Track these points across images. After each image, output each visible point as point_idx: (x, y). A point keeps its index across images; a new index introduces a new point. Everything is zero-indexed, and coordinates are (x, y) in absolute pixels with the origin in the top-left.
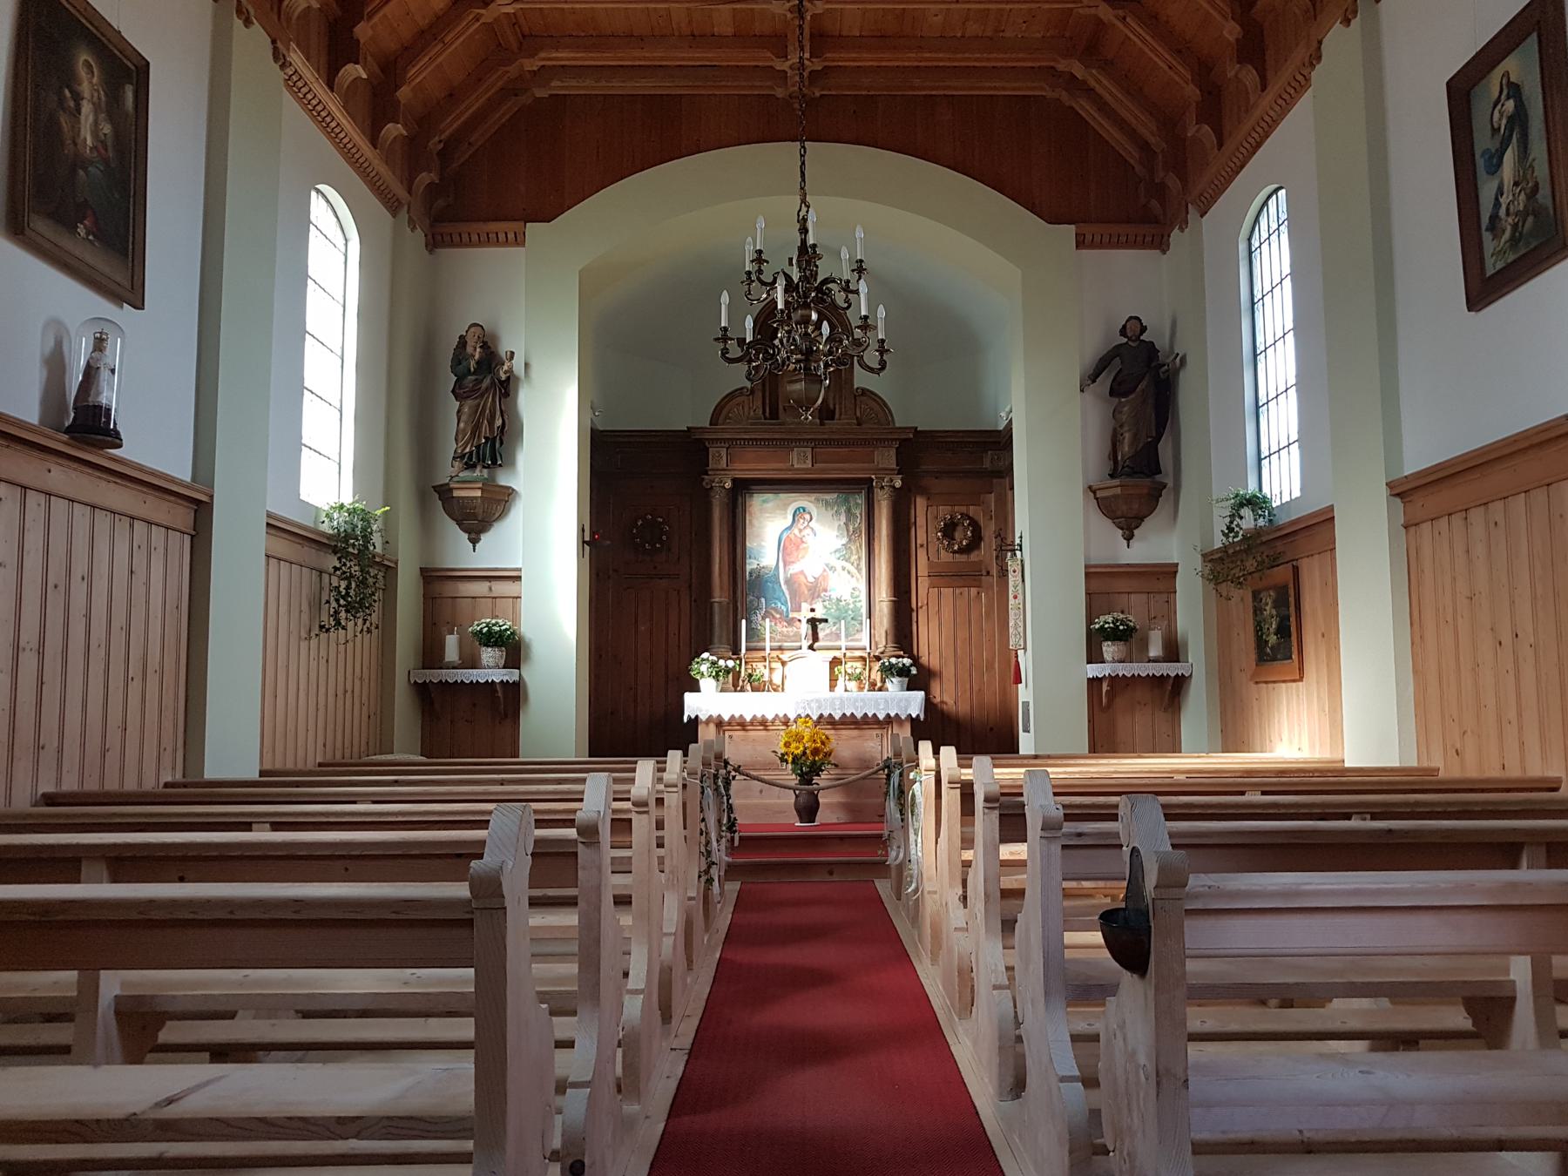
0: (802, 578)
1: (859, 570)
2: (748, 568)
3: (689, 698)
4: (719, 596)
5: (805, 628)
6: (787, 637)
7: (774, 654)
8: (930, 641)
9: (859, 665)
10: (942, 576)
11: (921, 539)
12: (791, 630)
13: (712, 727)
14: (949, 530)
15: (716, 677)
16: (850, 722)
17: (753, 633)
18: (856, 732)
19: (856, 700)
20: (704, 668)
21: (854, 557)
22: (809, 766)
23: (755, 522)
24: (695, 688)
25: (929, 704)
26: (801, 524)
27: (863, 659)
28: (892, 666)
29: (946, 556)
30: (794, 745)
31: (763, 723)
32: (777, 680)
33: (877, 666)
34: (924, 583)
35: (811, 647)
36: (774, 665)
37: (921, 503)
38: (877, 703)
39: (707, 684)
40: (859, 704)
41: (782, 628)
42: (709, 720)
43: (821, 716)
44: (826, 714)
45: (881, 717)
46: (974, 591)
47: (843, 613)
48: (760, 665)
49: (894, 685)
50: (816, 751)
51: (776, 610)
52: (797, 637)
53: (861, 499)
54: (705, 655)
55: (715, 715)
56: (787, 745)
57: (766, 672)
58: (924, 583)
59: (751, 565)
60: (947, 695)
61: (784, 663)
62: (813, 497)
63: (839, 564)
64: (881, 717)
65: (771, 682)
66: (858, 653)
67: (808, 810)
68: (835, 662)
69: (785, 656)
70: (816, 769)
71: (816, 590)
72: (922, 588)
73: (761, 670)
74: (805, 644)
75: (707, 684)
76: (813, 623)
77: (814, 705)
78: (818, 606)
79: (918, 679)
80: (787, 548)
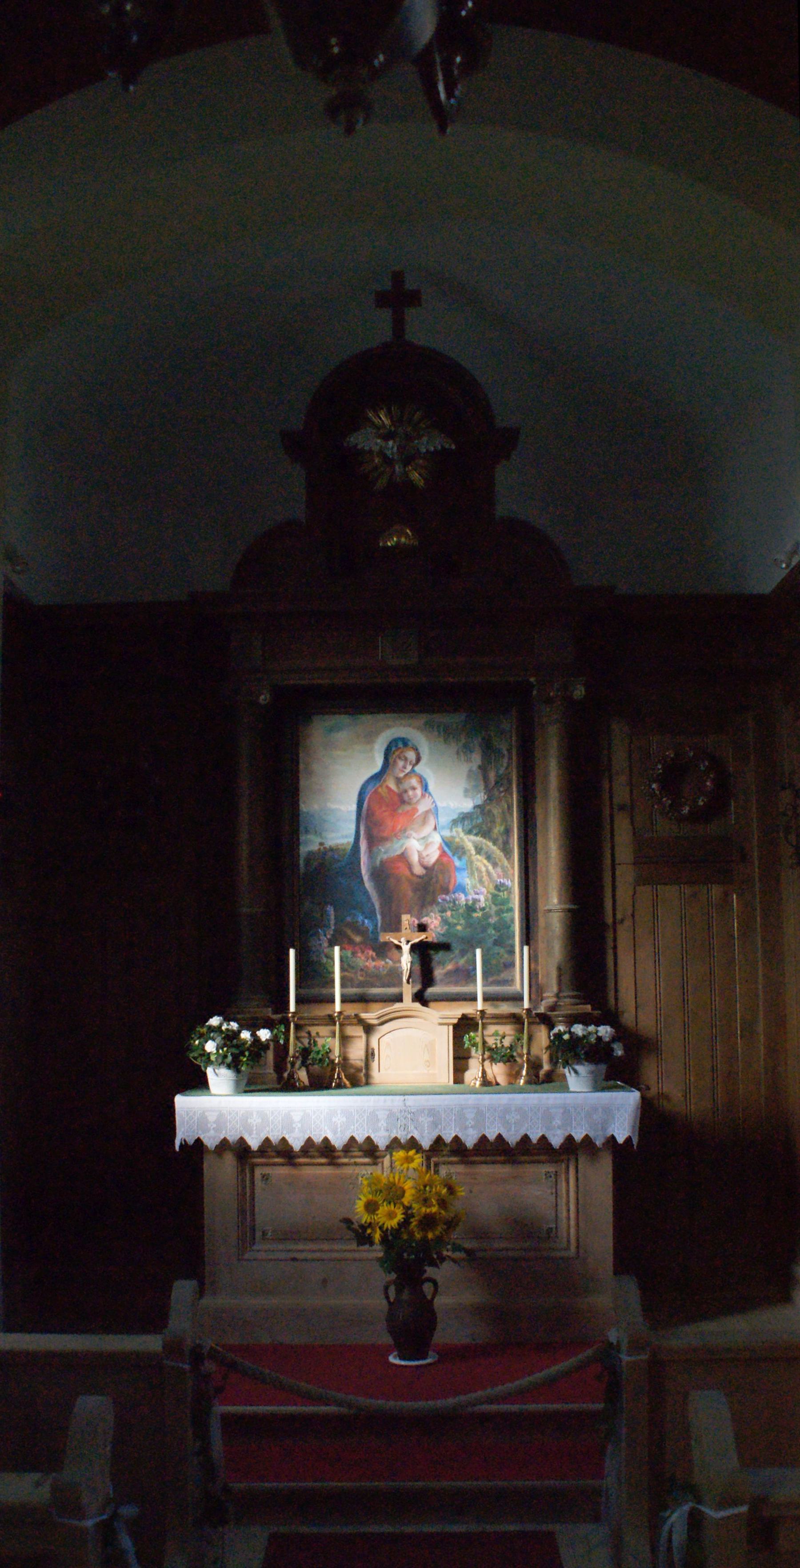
0: (404, 871)
1: (507, 851)
2: (304, 850)
3: (182, 1102)
4: (248, 906)
5: (406, 960)
6: (375, 978)
7: (352, 1010)
8: (640, 980)
9: (508, 1029)
10: (662, 863)
11: (621, 794)
12: (383, 965)
13: (229, 1159)
14: (673, 778)
15: (234, 1065)
16: (493, 1150)
17: (314, 974)
18: (504, 1170)
19: (507, 1110)
20: (210, 1047)
21: (498, 829)
22: (410, 1254)
23: (315, 767)
24: (199, 1083)
25: (650, 1114)
26: (401, 768)
27: (515, 1019)
28: (575, 1041)
29: (665, 828)
30: (384, 1209)
31: (326, 1150)
32: (356, 1053)
33: (542, 1037)
34: (626, 875)
35: (420, 998)
36: (351, 1031)
37: (619, 730)
38: (547, 1115)
39: (220, 1079)
40: (513, 1117)
41: (367, 961)
42: (224, 1145)
43: (439, 1140)
44: (448, 1138)
45: (556, 1141)
46: (716, 891)
47: (481, 930)
48: (324, 1030)
49: (578, 1080)
50: (428, 1222)
51: (358, 930)
52: (394, 977)
53: (508, 724)
54: (215, 1021)
55: (232, 1138)
56: (371, 1207)
57: (335, 1045)
58: (626, 875)
59: (309, 845)
60: (669, 1078)
61: (369, 1029)
62: (422, 719)
63: (469, 842)
64: (556, 1141)
65: (345, 1059)
66: (505, 1008)
67: (413, 1327)
68: (463, 1027)
69: (371, 1016)
70: (428, 1254)
71: (432, 885)
72: (623, 888)
73: (327, 1041)
74: (408, 991)
75: (220, 1079)
76: (422, 951)
77: (425, 1121)
78: (434, 921)
79: (617, 1067)
80: (380, 809)
